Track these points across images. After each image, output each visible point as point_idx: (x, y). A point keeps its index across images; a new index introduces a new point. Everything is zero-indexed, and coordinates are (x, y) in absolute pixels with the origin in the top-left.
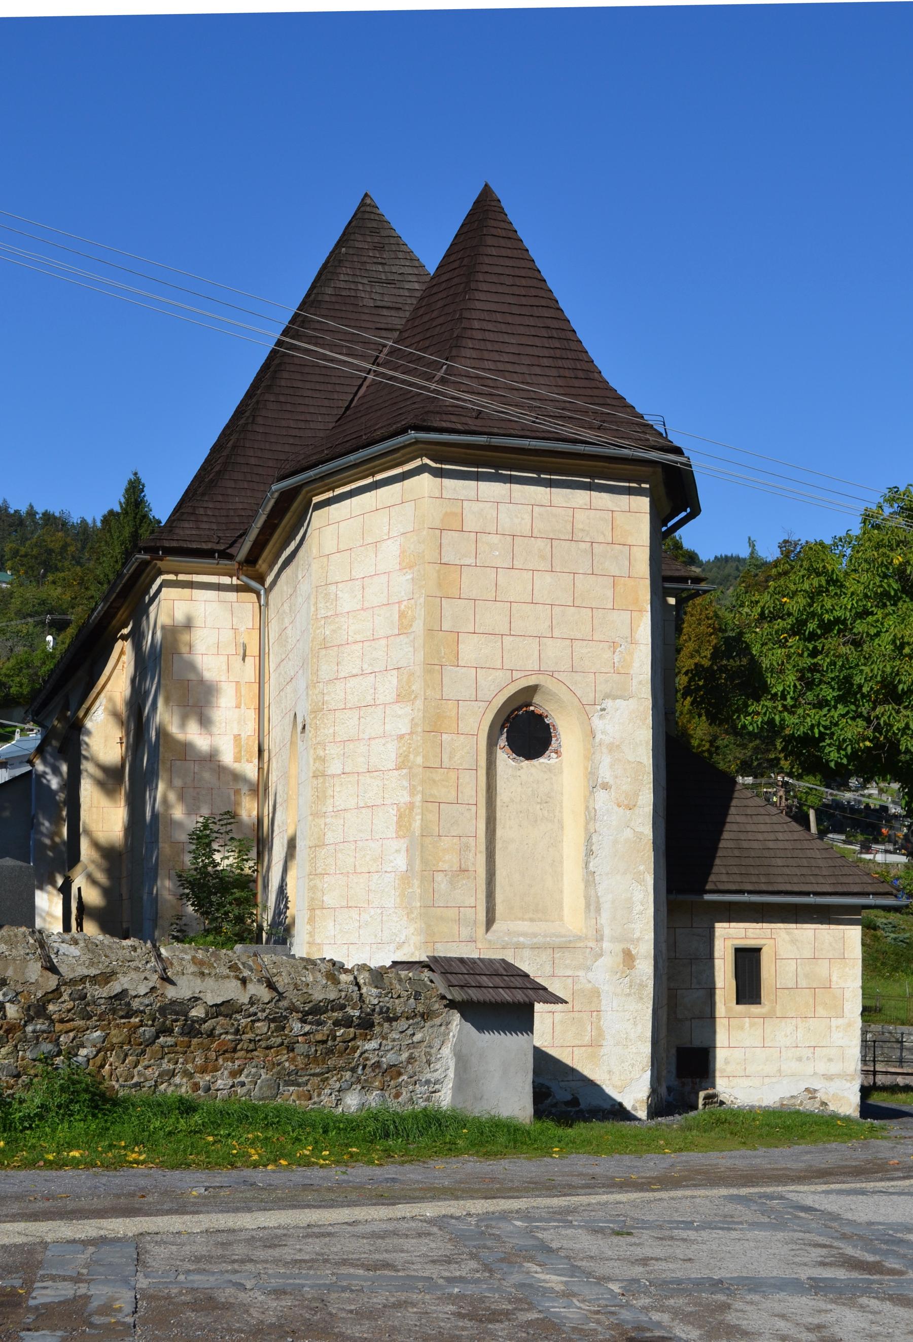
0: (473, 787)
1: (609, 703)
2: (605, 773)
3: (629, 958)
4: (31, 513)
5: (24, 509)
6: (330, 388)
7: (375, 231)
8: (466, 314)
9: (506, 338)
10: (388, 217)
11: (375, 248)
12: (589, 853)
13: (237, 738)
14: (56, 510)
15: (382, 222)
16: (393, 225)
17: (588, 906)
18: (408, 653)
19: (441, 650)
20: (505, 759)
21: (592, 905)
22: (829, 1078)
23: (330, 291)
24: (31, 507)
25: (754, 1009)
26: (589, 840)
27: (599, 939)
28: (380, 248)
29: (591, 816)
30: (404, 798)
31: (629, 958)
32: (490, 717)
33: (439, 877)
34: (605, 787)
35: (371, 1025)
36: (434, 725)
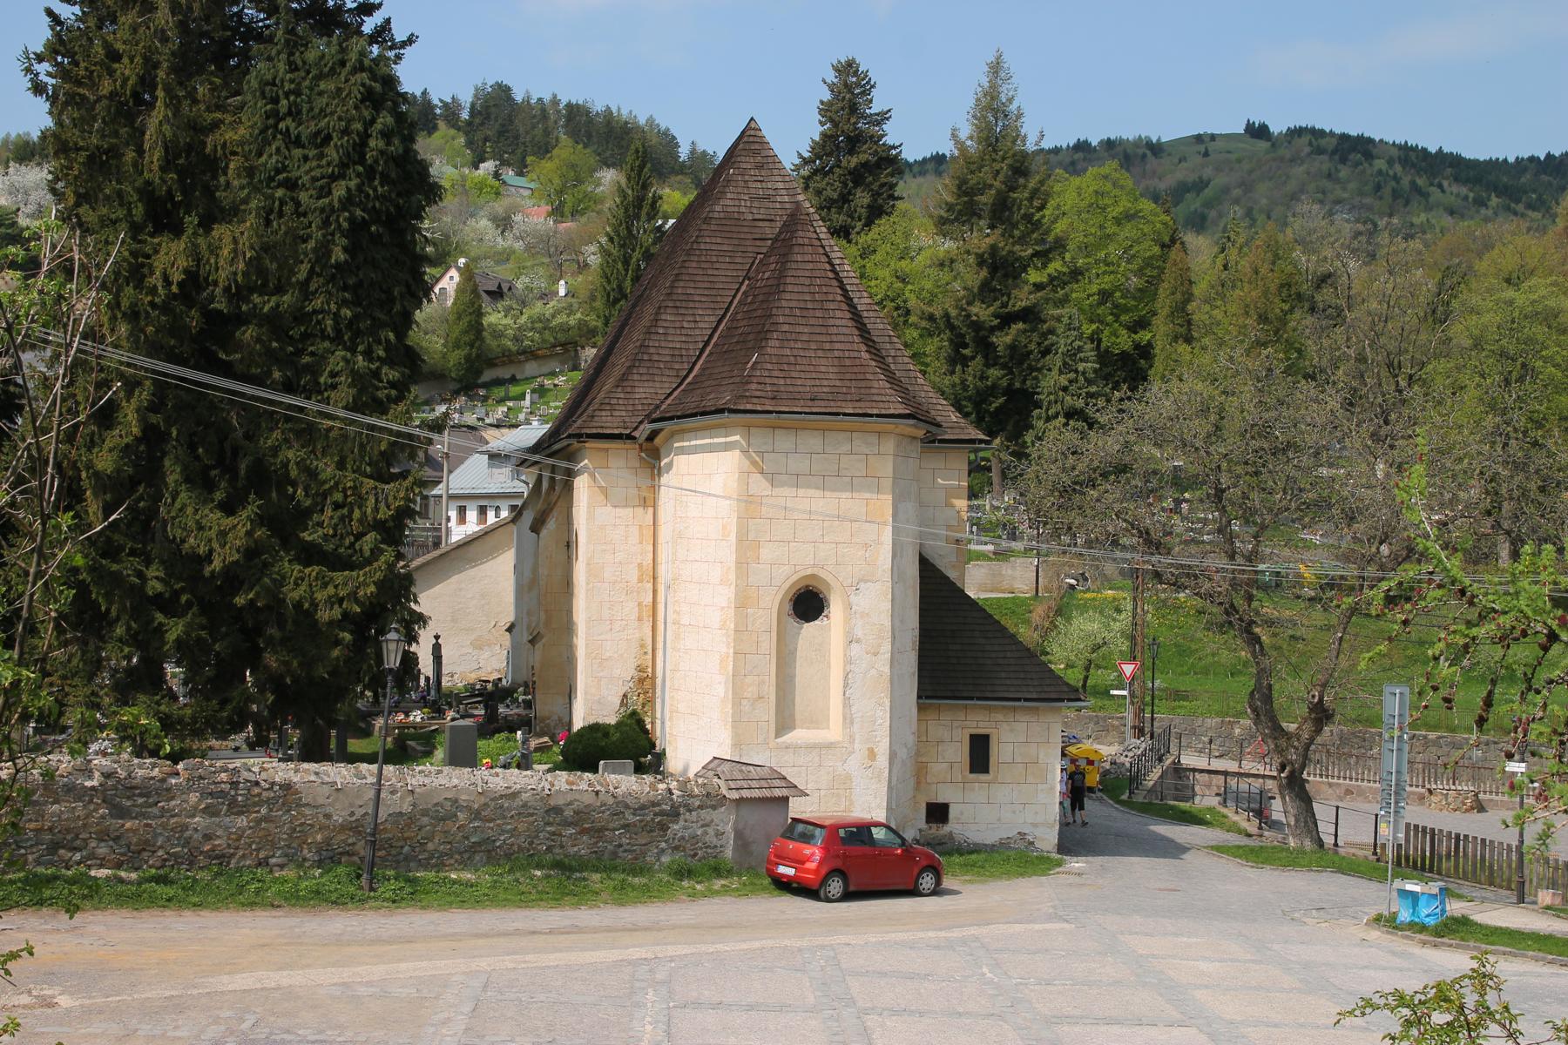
0: (769, 643)
1: (862, 585)
2: (859, 633)
3: (872, 755)
4: (555, 101)
5: (547, 97)
6: (714, 292)
7: (756, 153)
8: (774, 311)
9: (801, 329)
10: (768, 139)
11: (757, 167)
12: (846, 686)
13: (640, 565)
14: (577, 98)
15: (763, 143)
16: (772, 145)
17: (845, 718)
18: (728, 554)
19: (747, 547)
20: (792, 623)
21: (848, 720)
22: (1035, 825)
23: (718, 208)
24: (555, 96)
25: (983, 777)
26: (846, 677)
27: (852, 741)
28: (760, 167)
29: (848, 661)
30: (724, 650)
31: (872, 755)
32: (780, 596)
33: (744, 702)
34: (858, 641)
35: (678, 815)
36: (743, 602)
